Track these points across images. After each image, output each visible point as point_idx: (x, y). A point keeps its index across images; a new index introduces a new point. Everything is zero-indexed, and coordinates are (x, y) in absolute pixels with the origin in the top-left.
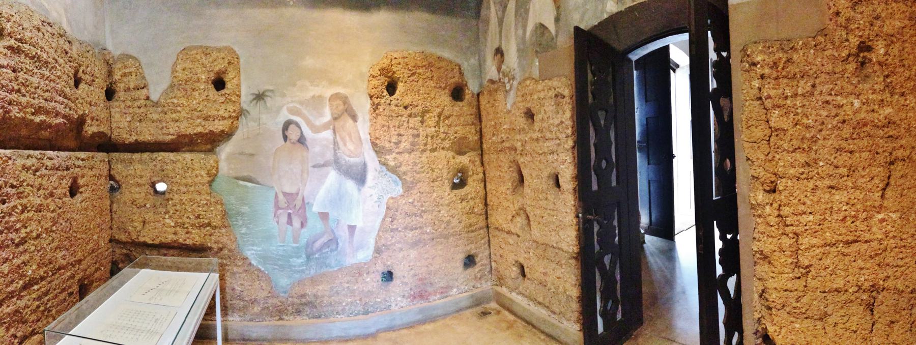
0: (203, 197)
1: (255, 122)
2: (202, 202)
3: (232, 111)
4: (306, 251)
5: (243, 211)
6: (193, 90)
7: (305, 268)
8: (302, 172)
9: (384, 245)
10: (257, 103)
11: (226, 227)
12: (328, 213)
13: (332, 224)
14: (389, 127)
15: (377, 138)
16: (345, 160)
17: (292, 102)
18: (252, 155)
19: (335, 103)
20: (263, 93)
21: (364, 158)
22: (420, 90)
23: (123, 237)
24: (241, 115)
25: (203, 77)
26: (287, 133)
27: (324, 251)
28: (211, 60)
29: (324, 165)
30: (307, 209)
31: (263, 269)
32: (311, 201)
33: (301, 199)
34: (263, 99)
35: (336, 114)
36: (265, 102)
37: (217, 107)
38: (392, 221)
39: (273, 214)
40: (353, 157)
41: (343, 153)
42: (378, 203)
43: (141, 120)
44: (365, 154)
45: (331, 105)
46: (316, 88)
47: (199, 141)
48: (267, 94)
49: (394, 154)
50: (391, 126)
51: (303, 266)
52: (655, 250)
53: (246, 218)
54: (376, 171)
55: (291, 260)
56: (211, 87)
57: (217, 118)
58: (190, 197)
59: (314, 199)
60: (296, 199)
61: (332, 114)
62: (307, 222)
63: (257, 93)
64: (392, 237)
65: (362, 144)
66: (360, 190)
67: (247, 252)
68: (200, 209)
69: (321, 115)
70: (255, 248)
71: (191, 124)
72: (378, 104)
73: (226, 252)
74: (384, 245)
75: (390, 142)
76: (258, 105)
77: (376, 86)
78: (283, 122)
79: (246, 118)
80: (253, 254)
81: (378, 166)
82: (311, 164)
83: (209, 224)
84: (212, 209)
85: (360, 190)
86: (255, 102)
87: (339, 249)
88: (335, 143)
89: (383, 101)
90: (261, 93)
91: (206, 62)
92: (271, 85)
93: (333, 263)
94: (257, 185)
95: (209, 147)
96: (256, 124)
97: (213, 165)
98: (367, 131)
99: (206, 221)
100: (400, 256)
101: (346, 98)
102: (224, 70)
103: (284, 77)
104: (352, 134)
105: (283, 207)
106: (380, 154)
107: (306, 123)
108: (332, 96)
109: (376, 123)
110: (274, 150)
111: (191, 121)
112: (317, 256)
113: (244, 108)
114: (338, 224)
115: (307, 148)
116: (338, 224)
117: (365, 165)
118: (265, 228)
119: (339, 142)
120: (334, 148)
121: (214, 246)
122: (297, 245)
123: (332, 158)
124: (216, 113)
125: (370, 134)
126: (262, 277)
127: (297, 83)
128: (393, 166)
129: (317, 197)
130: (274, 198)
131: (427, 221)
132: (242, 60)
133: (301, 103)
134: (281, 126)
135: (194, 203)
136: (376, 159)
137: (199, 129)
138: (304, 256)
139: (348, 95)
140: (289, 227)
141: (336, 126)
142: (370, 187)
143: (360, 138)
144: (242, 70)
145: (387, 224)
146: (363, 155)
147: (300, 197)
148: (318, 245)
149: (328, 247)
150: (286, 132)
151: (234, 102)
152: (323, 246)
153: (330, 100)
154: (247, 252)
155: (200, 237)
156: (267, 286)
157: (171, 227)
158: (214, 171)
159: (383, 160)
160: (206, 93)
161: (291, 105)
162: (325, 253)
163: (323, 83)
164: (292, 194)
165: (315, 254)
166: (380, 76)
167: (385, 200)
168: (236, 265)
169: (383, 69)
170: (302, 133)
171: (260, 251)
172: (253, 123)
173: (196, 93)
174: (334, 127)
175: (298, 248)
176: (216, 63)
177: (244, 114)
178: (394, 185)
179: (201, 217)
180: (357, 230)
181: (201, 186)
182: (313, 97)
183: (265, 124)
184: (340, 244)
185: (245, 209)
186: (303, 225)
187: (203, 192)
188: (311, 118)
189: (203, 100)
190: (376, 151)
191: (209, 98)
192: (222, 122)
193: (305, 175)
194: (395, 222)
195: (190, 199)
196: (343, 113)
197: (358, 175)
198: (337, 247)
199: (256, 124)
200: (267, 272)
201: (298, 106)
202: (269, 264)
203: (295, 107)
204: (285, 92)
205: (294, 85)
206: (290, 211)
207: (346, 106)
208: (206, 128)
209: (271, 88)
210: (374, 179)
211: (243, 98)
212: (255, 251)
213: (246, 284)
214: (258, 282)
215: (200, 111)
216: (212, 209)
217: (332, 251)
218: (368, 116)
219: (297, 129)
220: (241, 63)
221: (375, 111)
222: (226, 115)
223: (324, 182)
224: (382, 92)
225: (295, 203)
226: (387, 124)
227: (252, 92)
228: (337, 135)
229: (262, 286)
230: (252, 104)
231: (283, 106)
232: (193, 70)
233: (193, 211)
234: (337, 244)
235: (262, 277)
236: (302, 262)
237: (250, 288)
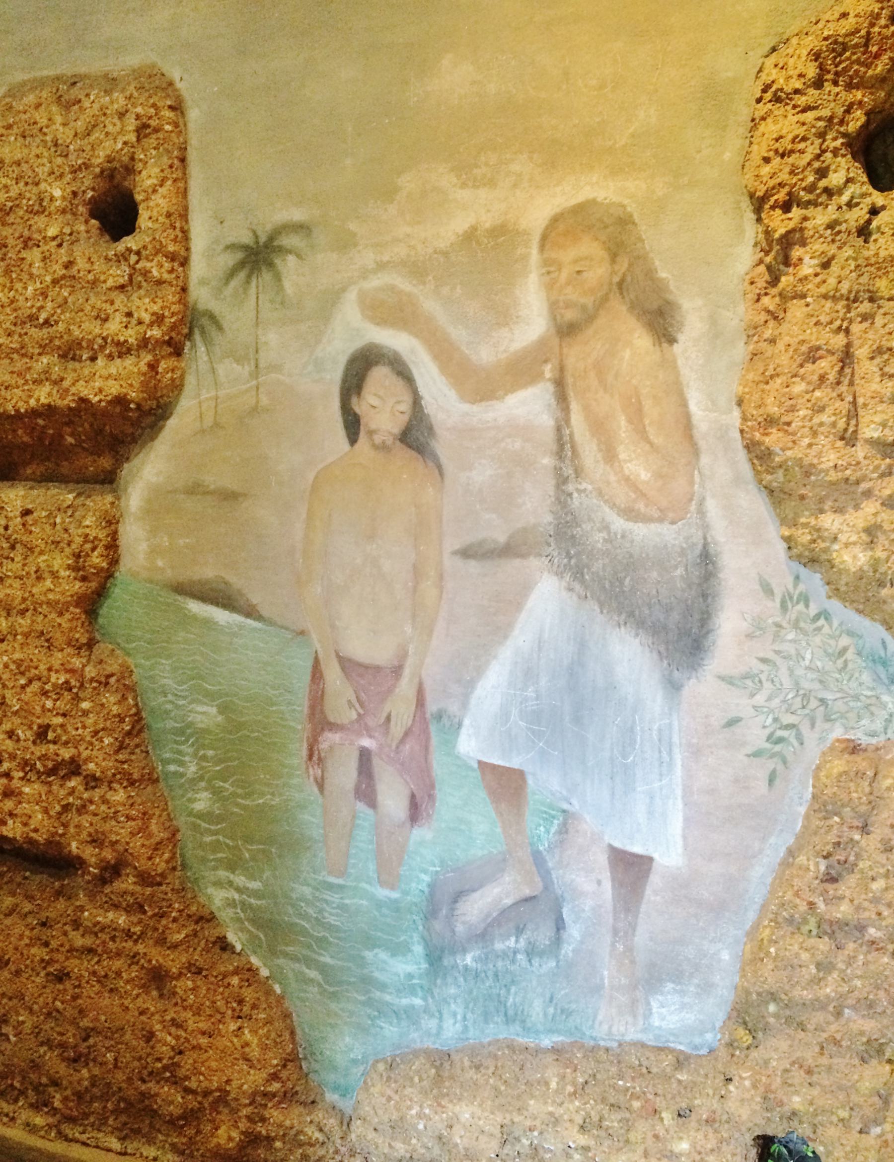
0: (57, 658)
3: (147, 318)
6: (27, 243)
7: (418, 1002)
8: (417, 572)
10: (248, 281)
11: (132, 783)
14: (846, 357)
15: (770, 421)
16: (606, 527)
17: (381, 266)
18: (230, 497)
19: (567, 256)
20: (271, 239)
21: (706, 528)
24: (189, 336)
25: (57, 193)
26: (359, 407)
27: (499, 946)
28: (80, 125)
30: (435, 740)
32: (453, 708)
33: (412, 694)
34: (271, 265)
35: (568, 305)
36: (278, 278)
37: (99, 304)
38: (831, 879)
39: (304, 753)
40: (647, 519)
41: (600, 494)
42: (770, 765)
44: (712, 506)
45: (550, 266)
49: (870, 507)
50: (861, 352)
51: (412, 991)
52: (263, 268)
54: (768, 591)
55: (369, 955)
57: (102, 348)
58: (17, 656)
59: (465, 705)
61: (553, 307)
62: (431, 797)
63: (246, 238)
64: (824, 967)
65: (696, 452)
66: (673, 687)
67: (210, 890)
68: (49, 704)
70: (240, 880)
71: (20, 374)
72: (788, 241)
75: (848, 438)
76: (253, 290)
77: (786, 144)
79: (208, 342)
80: (232, 904)
82: (452, 543)
83: (74, 768)
84: (85, 705)
87: (567, 950)
89: (820, 218)
90: (263, 239)
91: (64, 134)
93: (537, 1010)
94: (249, 621)
95: (105, 462)
96: (245, 370)
97: (93, 533)
99: (66, 754)
100: (866, 1085)
101: (625, 222)
102: (125, 159)
103: (348, 162)
106: (791, 505)
107: (436, 357)
108: (556, 220)
109: (772, 341)
110: (311, 476)
111: (20, 364)
112: (469, 959)
113: (201, 306)
114: (564, 830)
115: (439, 467)
116: (564, 830)
119: (578, 437)
120: (558, 470)
121: (89, 854)
122: (395, 895)
123: (549, 518)
124: (96, 328)
125: (740, 403)
126: (254, 1007)
128: (860, 576)
130: (308, 678)
132: (194, 115)
134: (335, 375)
135: (30, 681)
136: (773, 532)
137: (43, 395)
138: (418, 949)
141: (571, 362)
142: (728, 680)
143: (688, 416)
144: (192, 156)
146: (701, 512)
147: (406, 687)
150: (354, 400)
151: (160, 282)
153: (544, 238)
154: (210, 890)
155: (46, 811)
158: (97, 559)
160: (63, 255)
161: (375, 282)
162: (504, 955)
163: (515, 167)
164: (378, 669)
165: (464, 951)
166: (818, 84)
167: (813, 752)
168: (161, 941)
169: (839, 47)
170: (417, 401)
171: (256, 894)
172: (237, 368)
173: (34, 255)
174: (562, 369)
175: (395, 907)
176: (96, 135)
177: (203, 332)
178: (866, 677)
179: (51, 736)
180: (655, 880)
181: (53, 615)
182: (470, 236)
184: (574, 932)
187: (59, 639)
188: (458, 334)
189: (55, 282)
190: (771, 492)
191: (74, 271)
192: (117, 366)
194: (848, 886)
195: (19, 663)
196: (605, 299)
198: (558, 941)
199: (245, 370)
200: (278, 989)
201: (404, 284)
203: (392, 288)
204: (352, 226)
205: (389, 193)
206: (366, 742)
207: (623, 264)
208: (67, 391)
209: (297, 215)
210: (750, 636)
211: (198, 268)
212: (238, 890)
213: (191, 1025)
214: (233, 1026)
216: (85, 705)
217: (531, 952)
218: (741, 309)
219: (399, 384)
220: (191, 126)
221: (774, 281)
222: (131, 336)
223: (510, 626)
224: (822, 173)
225: (388, 707)
226: (840, 340)
227: (231, 240)
228: (574, 406)
229: (247, 1044)
231: (344, 290)
232: (25, 167)
233: (25, 712)
234: (560, 925)
235: (254, 1007)
236: (410, 976)
237: (204, 1041)
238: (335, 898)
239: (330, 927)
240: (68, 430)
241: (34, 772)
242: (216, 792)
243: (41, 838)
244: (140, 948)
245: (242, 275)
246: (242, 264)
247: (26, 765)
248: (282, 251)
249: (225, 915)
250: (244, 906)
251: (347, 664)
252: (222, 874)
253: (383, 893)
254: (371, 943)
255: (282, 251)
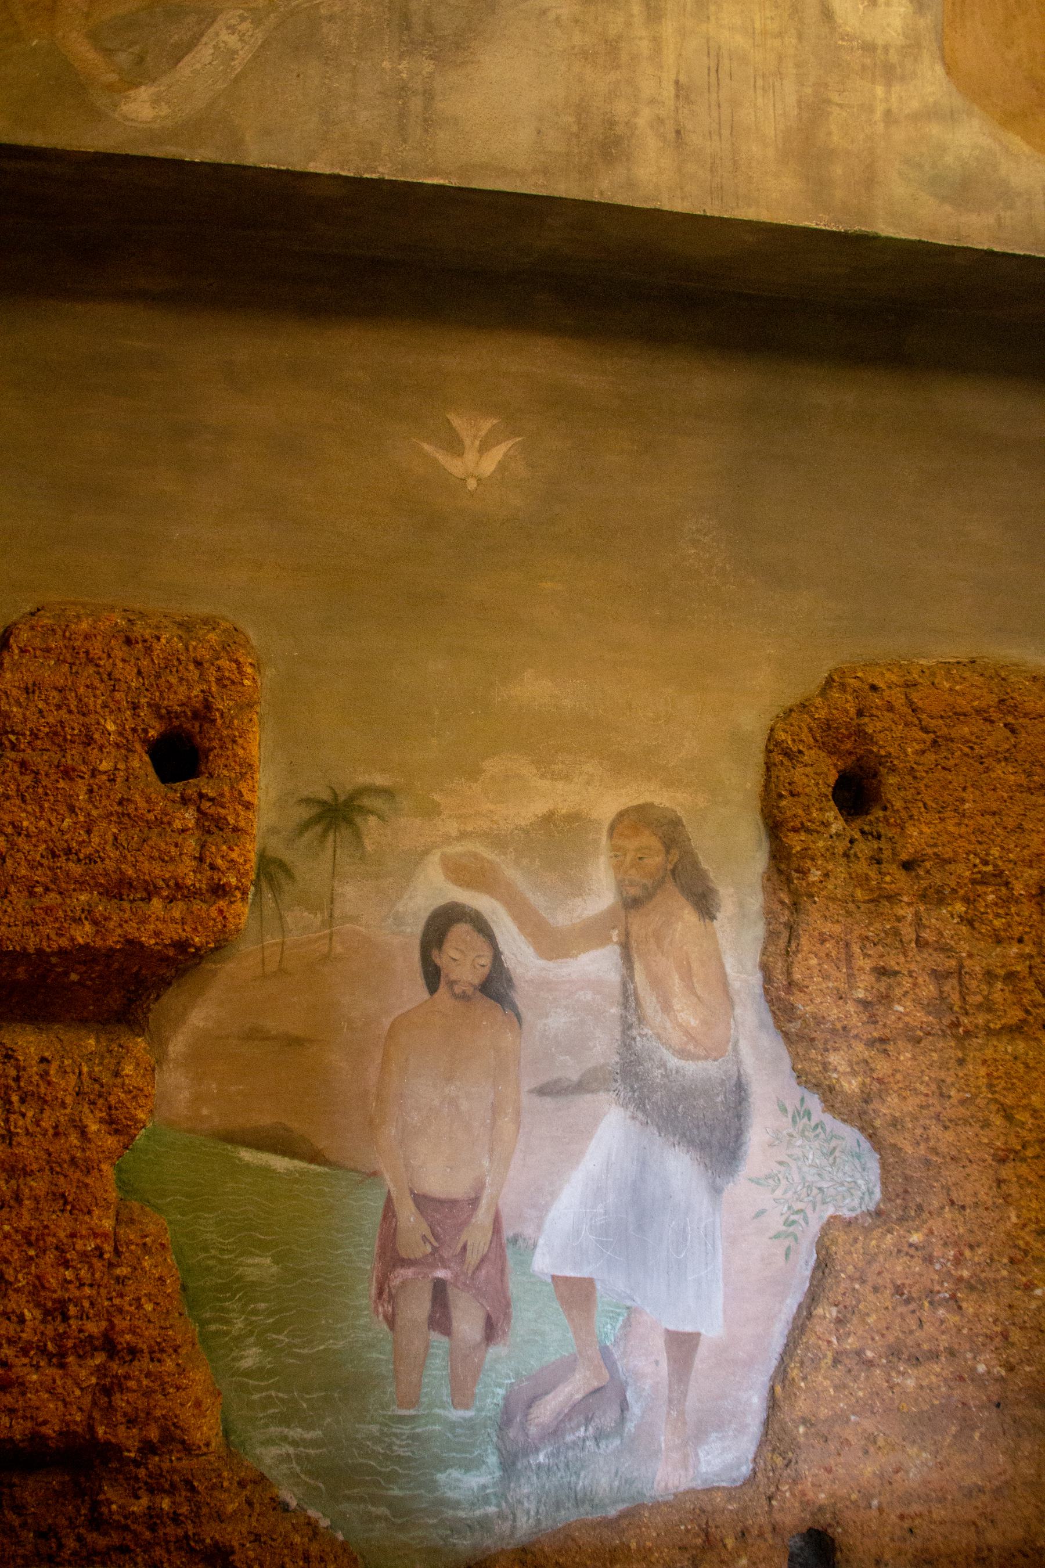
1: (313, 909)
2: (79, 1245)
4: (501, 1438)
5: (251, 1274)
8: (496, 1110)
9: (805, 1421)
10: (326, 831)
12: (590, 1282)
13: (607, 1329)
16: (663, 1065)
17: (463, 836)
18: (294, 1042)
19: (632, 845)
20: (351, 798)
21: (739, 1063)
22: (963, 801)
26: (441, 960)
27: (569, 1438)
29: (580, 1087)
30: (510, 1263)
32: (529, 1231)
34: (350, 822)
35: (632, 884)
41: (659, 1037)
42: (787, 1243)
45: (617, 851)
46: (560, 785)
47: (74, 977)
48: (366, 802)
53: (262, 1306)
56: (141, 762)
59: (539, 1227)
60: (466, 1223)
61: (620, 885)
62: (507, 1316)
63: (325, 795)
65: (732, 1005)
66: (716, 1191)
69: (578, 888)
74: (805, 1421)
76: (331, 837)
78: (424, 916)
81: (794, 1093)
82: (528, 1083)
85: (716, 1191)
86: (318, 829)
87: (630, 1427)
88: (628, 997)
90: (342, 798)
92: (383, 770)
98: (752, 956)
101: (676, 823)
104: (695, 966)
105: (418, 1255)
108: (621, 815)
112: (541, 1458)
114: (627, 1324)
115: (518, 1016)
117: (740, 1089)
118: (340, 1344)
120: (623, 1019)
122: (470, 1414)
127: (487, 764)
129: (552, 1214)
130: (379, 1218)
131: (978, 1328)
133: (499, 841)
134: (415, 929)
137: (83, 934)
138: (493, 1460)
139: (681, 813)
140: (435, 1336)
141: (634, 929)
142: (756, 1181)
145: (819, 1329)
146: (736, 1050)
147: (483, 1217)
148: (547, 1410)
149: (588, 1421)
150: (435, 953)
152: (569, 1417)
153: (612, 828)
161: (459, 848)
164: (453, 1203)
165: (537, 1450)
170: (497, 955)
171: (315, 1443)
174: (627, 935)
180: (702, 1351)
182: (548, 819)
183: (355, 919)
184: (636, 1409)
186: (491, 1330)
188: (537, 900)
190: (786, 1035)
193: (506, 1123)
197: (712, 1129)
198: (622, 1420)
200: (340, 1537)
202: (348, 1498)
203: (475, 855)
204: (436, 797)
205: (474, 773)
206: (441, 1274)
209: (380, 780)
212: (294, 1443)
215: (90, 859)
219: (479, 940)
223: (582, 1153)
228: (638, 966)
230: (308, 836)
231: (427, 852)
234: (624, 1406)
236: (484, 1487)
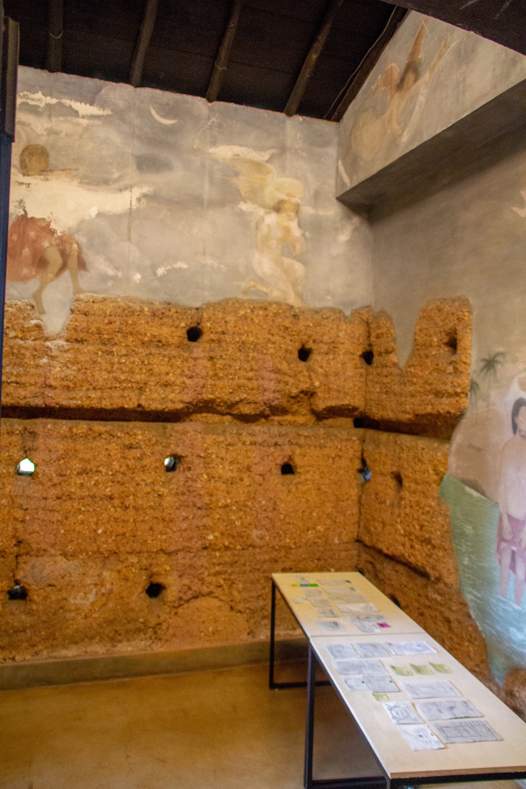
6: (427, 356)
23: (366, 539)
31: (480, 628)
34: (494, 367)
36: (495, 371)
39: (496, 549)
43: (387, 391)
63: (487, 357)
70: (475, 593)
73: (441, 585)
78: (513, 403)
80: (472, 600)
90: (492, 357)
99: (427, 536)
122: (520, 608)
134: (510, 408)
137: (429, 409)
150: (516, 419)
156: (475, 654)
157: (401, 534)
159: (250, 431)
168: (450, 609)
171: (478, 598)
173: (428, 361)
185: (468, 529)
206: (514, 548)
209: (501, 349)
212: (475, 596)
238: (501, 604)
239: (500, 616)
240: (438, 420)
241: (68, 434)
242: (470, 558)
243: (419, 564)
244: (443, 609)
245: (485, 370)
246: (485, 367)
247: (417, 537)
248: (497, 362)
249: (471, 604)
250: (477, 603)
251: (510, 518)
252: (470, 589)
253: (516, 607)
254: (512, 625)
255: (497, 362)
